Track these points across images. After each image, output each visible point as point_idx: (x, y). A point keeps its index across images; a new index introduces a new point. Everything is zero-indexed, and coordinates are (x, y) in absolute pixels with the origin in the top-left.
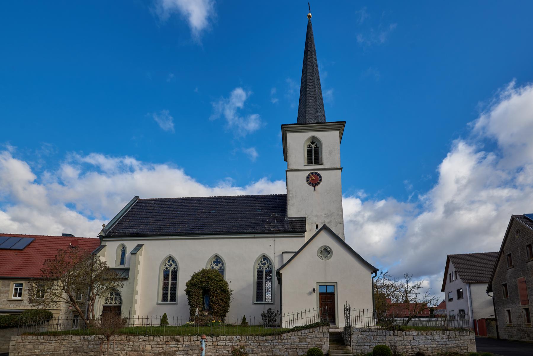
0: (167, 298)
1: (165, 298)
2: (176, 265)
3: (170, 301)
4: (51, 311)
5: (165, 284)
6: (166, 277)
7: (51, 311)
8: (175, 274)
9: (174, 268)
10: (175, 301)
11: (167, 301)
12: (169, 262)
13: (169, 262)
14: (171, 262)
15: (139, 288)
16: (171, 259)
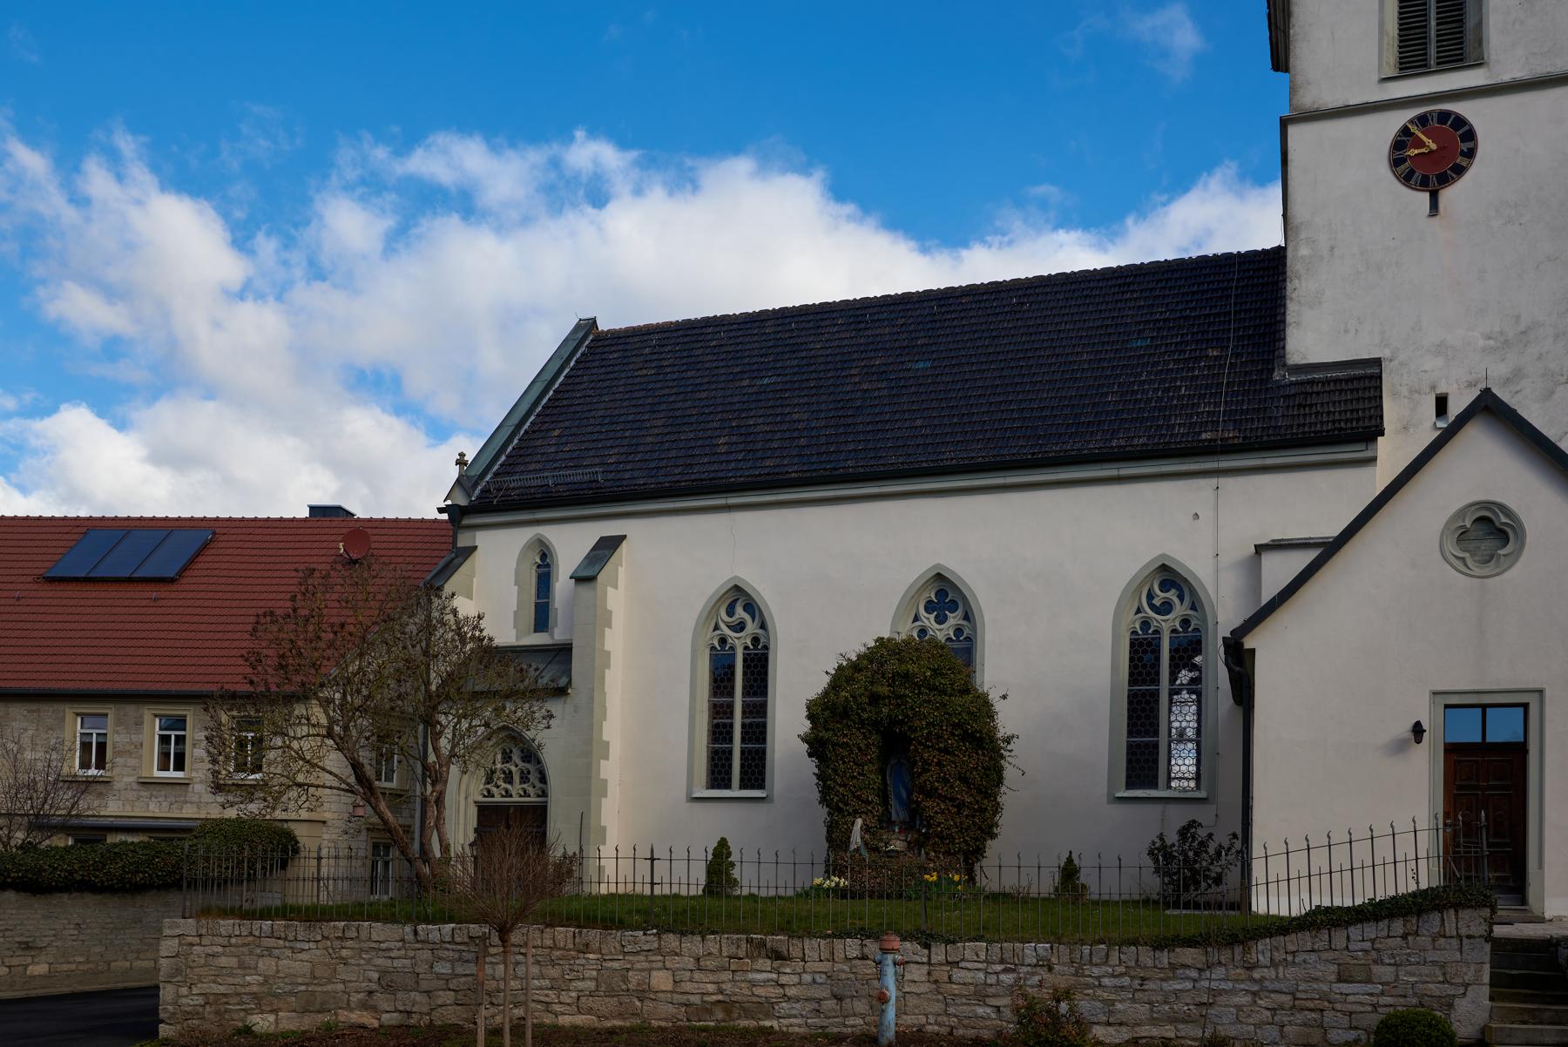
0: (729, 772)
1: (718, 775)
2: (763, 626)
3: (743, 786)
4: (292, 826)
5: (720, 712)
6: (721, 680)
7: (292, 826)
8: (758, 664)
9: (756, 640)
10: (761, 786)
11: (728, 786)
12: (730, 611)
13: (730, 611)
14: (740, 613)
15: (614, 728)
16: (739, 599)
